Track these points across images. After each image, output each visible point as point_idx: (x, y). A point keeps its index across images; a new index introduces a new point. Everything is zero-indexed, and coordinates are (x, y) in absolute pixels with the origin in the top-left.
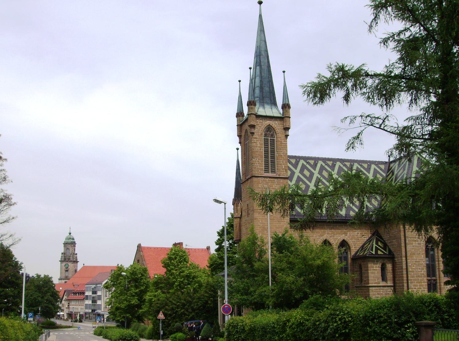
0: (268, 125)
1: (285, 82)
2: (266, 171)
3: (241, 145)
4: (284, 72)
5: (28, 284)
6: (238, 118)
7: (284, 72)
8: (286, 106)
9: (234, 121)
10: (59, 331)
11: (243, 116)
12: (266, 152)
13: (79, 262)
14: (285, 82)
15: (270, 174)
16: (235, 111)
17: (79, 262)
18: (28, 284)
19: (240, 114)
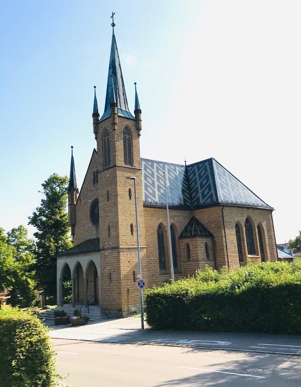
3: (97, 141)
8: (138, 111)
19: (96, 114)
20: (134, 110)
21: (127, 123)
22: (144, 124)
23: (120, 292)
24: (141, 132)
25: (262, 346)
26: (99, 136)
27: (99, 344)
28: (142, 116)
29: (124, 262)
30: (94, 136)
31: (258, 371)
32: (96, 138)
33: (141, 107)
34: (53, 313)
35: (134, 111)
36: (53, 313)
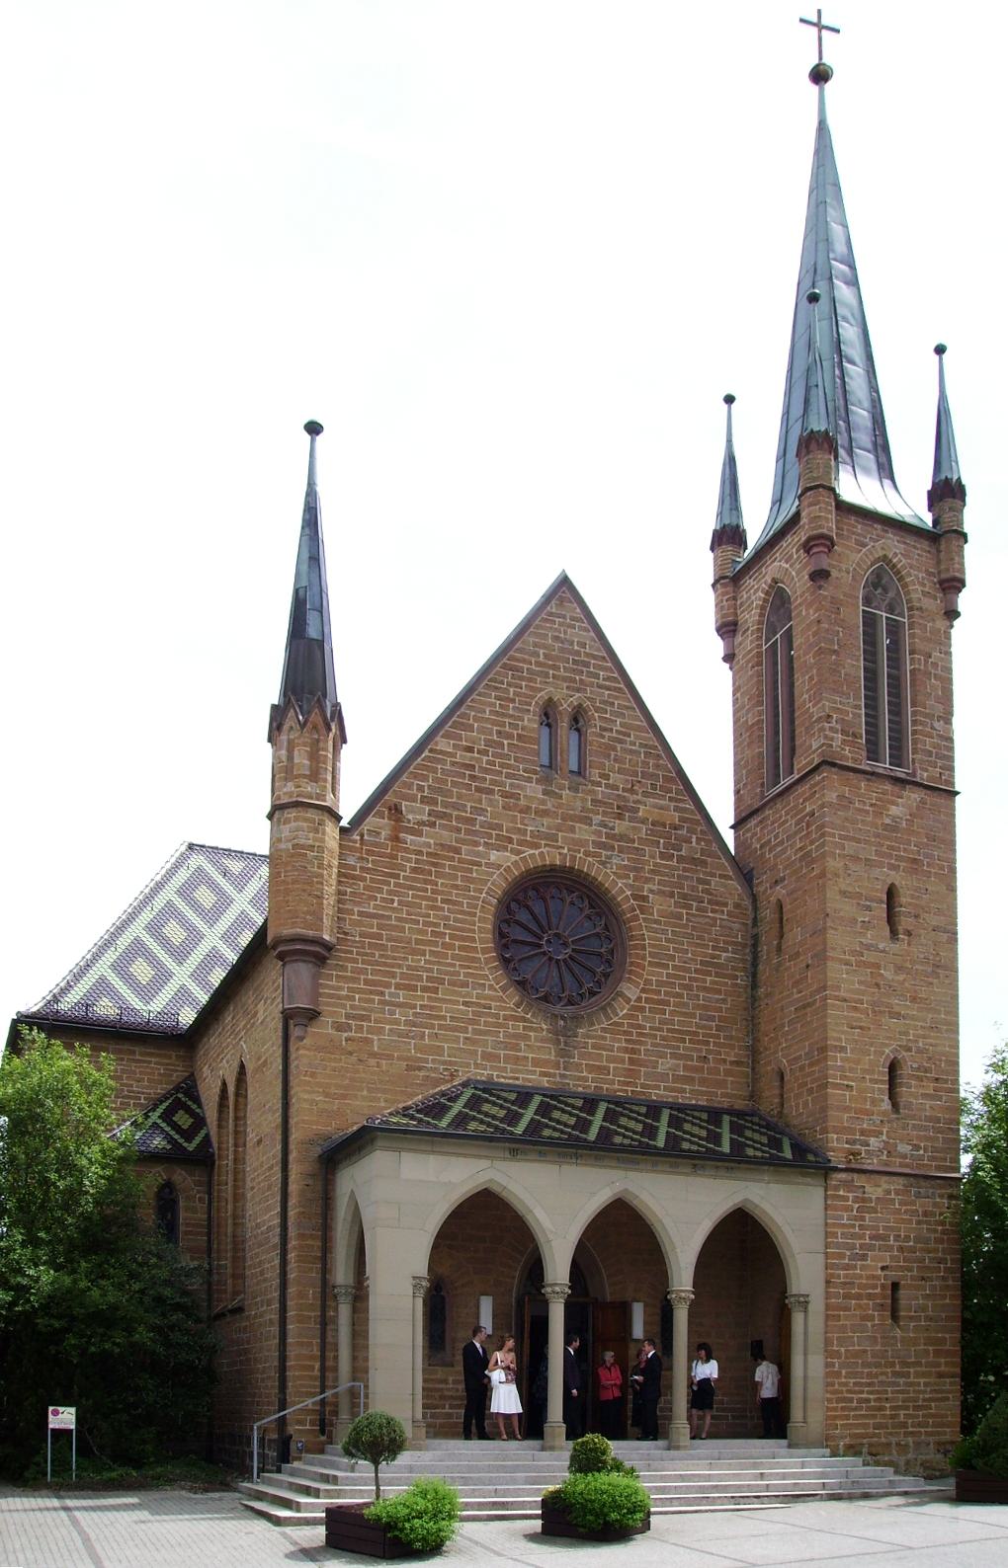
0: (878, 560)
1: (729, 441)
2: (873, 754)
3: (731, 668)
4: (314, 429)
5: (56, 1463)
6: (719, 551)
7: (314, 429)
8: (947, 492)
9: (704, 565)
10: (803, 1184)
11: (743, 543)
12: (871, 676)
13: (959, 793)
14: (729, 441)
15: (884, 766)
16: (709, 524)
17: (959, 793)
18: (56, 1463)
19: (728, 536)
20: (929, 488)
21: (893, 546)
22: (975, 560)
23: (949, 1018)
24: (964, 601)
25: (784, 1476)
26: (738, 811)
27: (781, 1186)
28: (973, 518)
29: (876, 1082)
30: (718, 646)
31: (341, 1299)
32: (729, 658)
33: (968, 472)
34: (321, 991)
35: (929, 492)
36: (321, 984)
